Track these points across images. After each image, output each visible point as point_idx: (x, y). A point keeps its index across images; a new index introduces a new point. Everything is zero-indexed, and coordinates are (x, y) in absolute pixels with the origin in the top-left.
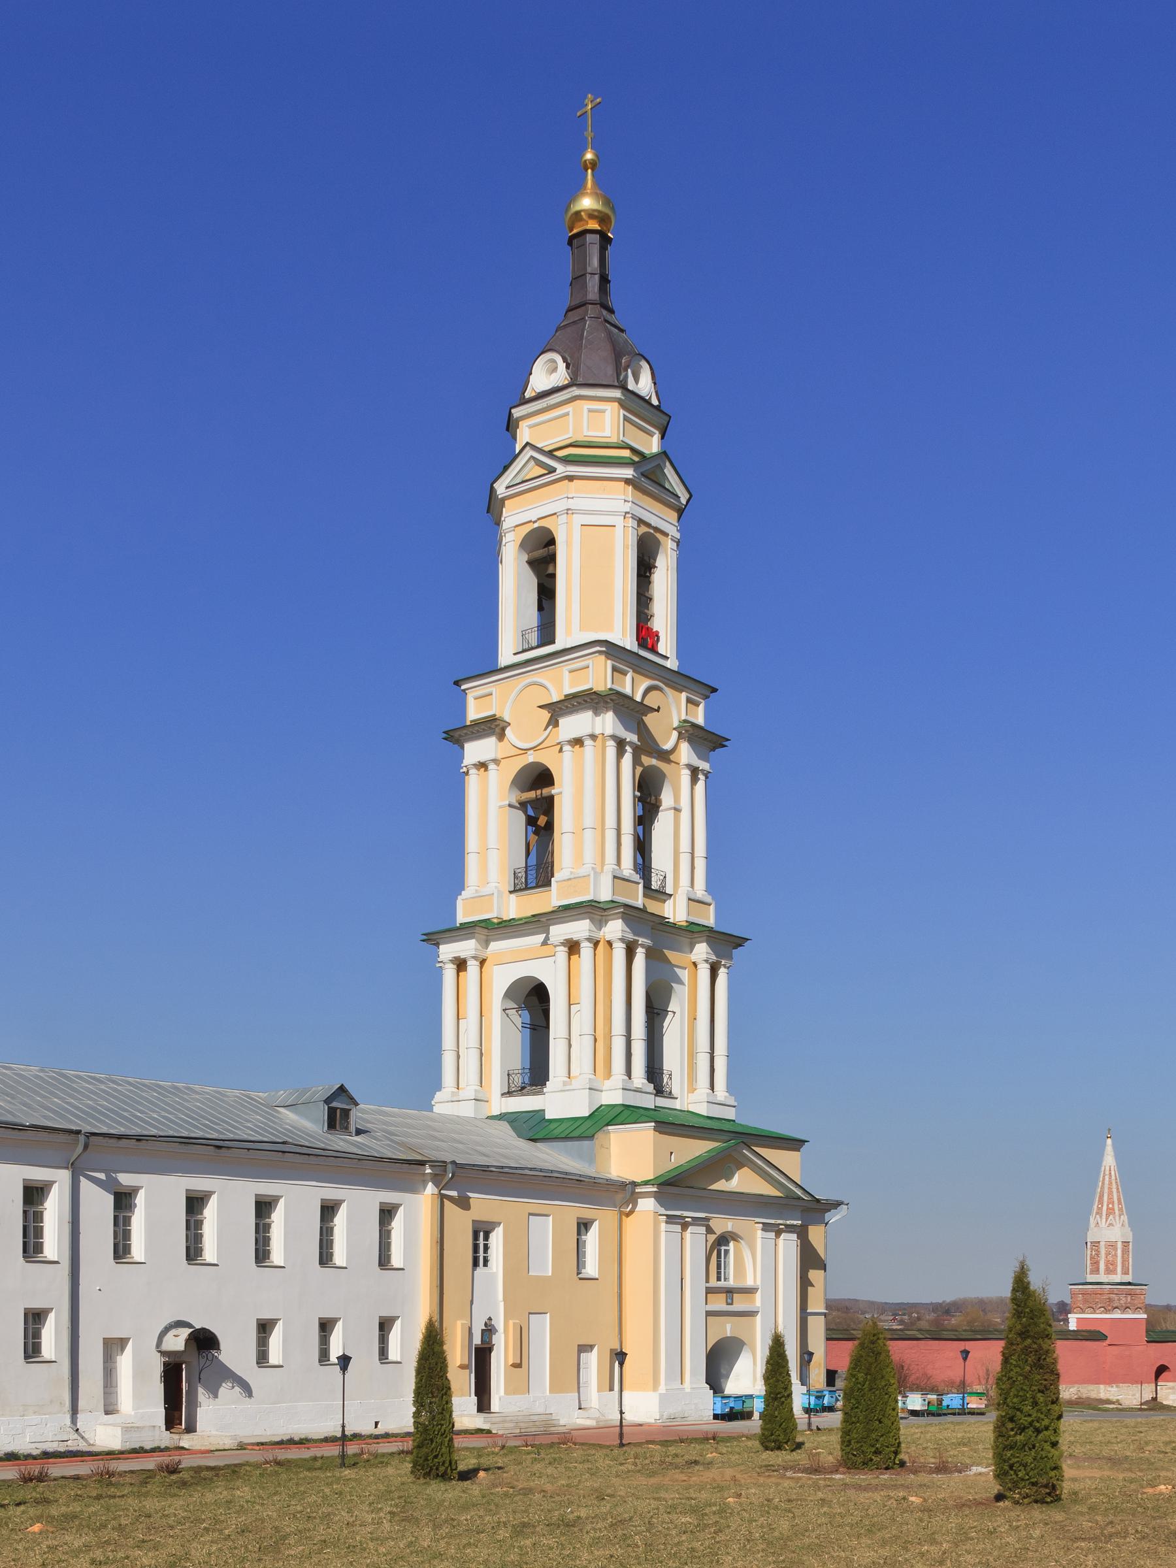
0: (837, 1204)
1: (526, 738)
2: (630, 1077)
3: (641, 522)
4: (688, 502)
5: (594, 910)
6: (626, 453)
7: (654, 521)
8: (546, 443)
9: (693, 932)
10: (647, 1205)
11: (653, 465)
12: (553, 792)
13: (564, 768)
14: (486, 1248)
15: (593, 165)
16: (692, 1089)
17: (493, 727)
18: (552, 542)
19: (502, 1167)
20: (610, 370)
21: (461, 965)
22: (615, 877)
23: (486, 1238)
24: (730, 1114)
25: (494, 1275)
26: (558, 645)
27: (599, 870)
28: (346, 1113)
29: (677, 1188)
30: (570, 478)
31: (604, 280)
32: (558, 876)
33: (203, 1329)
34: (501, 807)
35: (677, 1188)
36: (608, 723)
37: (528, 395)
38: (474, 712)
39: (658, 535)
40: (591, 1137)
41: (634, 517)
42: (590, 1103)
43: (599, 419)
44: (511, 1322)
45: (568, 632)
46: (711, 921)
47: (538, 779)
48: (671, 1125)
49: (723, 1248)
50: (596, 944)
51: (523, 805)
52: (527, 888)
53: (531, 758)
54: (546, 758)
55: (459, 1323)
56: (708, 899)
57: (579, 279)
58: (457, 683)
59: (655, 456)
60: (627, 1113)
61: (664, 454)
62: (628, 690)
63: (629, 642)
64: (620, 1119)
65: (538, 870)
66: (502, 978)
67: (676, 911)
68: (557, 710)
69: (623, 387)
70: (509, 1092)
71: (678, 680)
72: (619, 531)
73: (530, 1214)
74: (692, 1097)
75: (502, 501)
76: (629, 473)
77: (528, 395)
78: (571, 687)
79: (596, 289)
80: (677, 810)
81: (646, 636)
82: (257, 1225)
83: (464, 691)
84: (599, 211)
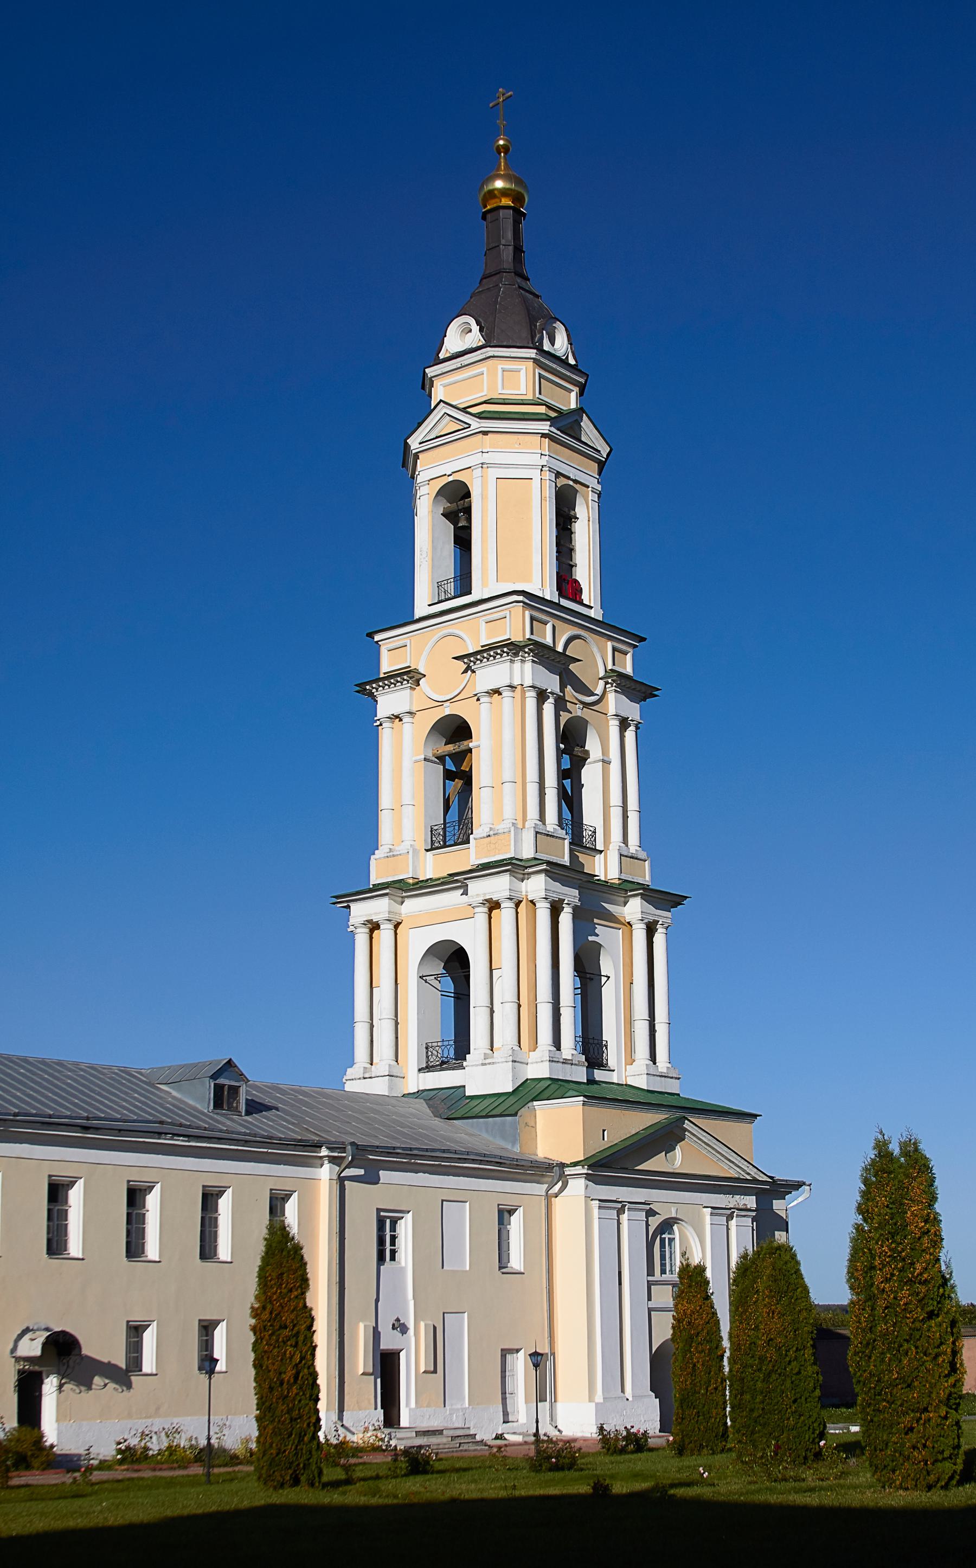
0: (798, 1186)
1: (442, 690)
2: (559, 1049)
3: (558, 474)
4: (608, 455)
5: (516, 867)
6: (542, 409)
7: (573, 474)
8: (462, 402)
9: (625, 889)
10: (577, 1187)
11: (570, 420)
12: (471, 745)
13: (482, 721)
14: (393, 1238)
15: (506, 149)
16: (631, 1061)
17: (411, 676)
18: (468, 495)
19: (411, 1149)
20: (525, 333)
21: (374, 927)
22: (537, 833)
23: (393, 1229)
24: (672, 1087)
25: (403, 1270)
26: (475, 596)
27: (520, 826)
28: (234, 1090)
29: (609, 1166)
30: (485, 433)
31: (518, 250)
32: (479, 831)
33: (63, 1332)
34: (416, 762)
35: (609, 1166)
36: (525, 672)
37: (441, 356)
38: (387, 665)
39: (577, 487)
40: (515, 1114)
41: (551, 469)
42: (514, 1078)
43: (512, 375)
44: (422, 1324)
45: (484, 584)
46: (647, 879)
47: (456, 731)
48: (597, 1094)
49: (666, 1236)
50: (518, 904)
51: (441, 759)
52: (445, 846)
53: (447, 710)
54: (462, 710)
55: (361, 1326)
56: (643, 855)
57: (493, 249)
58: (370, 635)
59: (574, 411)
60: (554, 1087)
61: (580, 411)
62: (549, 641)
63: (549, 592)
64: (546, 1094)
65: (455, 823)
66: (418, 943)
67: (606, 867)
68: (470, 661)
69: (540, 350)
70: (427, 1067)
71: (605, 628)
72: (536, 483)
73: (443, 1201)
74: (628, 1069)
75: (416, 456)
76: (545, 427)
77: (441, 356)
78: (488, 638)
79: (511, 257)
80: (606, 762)
81: (567, 584)
82: (129, 1215)
83: (377, 642)
84: (508, 189)
